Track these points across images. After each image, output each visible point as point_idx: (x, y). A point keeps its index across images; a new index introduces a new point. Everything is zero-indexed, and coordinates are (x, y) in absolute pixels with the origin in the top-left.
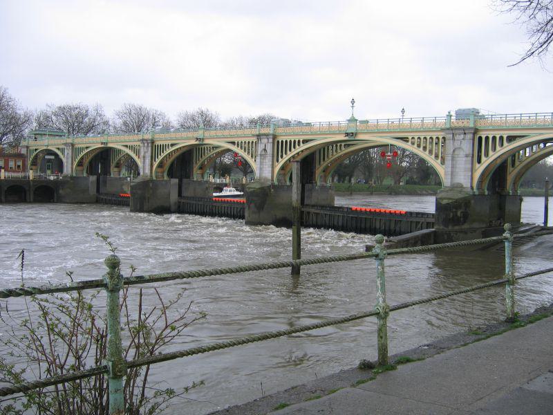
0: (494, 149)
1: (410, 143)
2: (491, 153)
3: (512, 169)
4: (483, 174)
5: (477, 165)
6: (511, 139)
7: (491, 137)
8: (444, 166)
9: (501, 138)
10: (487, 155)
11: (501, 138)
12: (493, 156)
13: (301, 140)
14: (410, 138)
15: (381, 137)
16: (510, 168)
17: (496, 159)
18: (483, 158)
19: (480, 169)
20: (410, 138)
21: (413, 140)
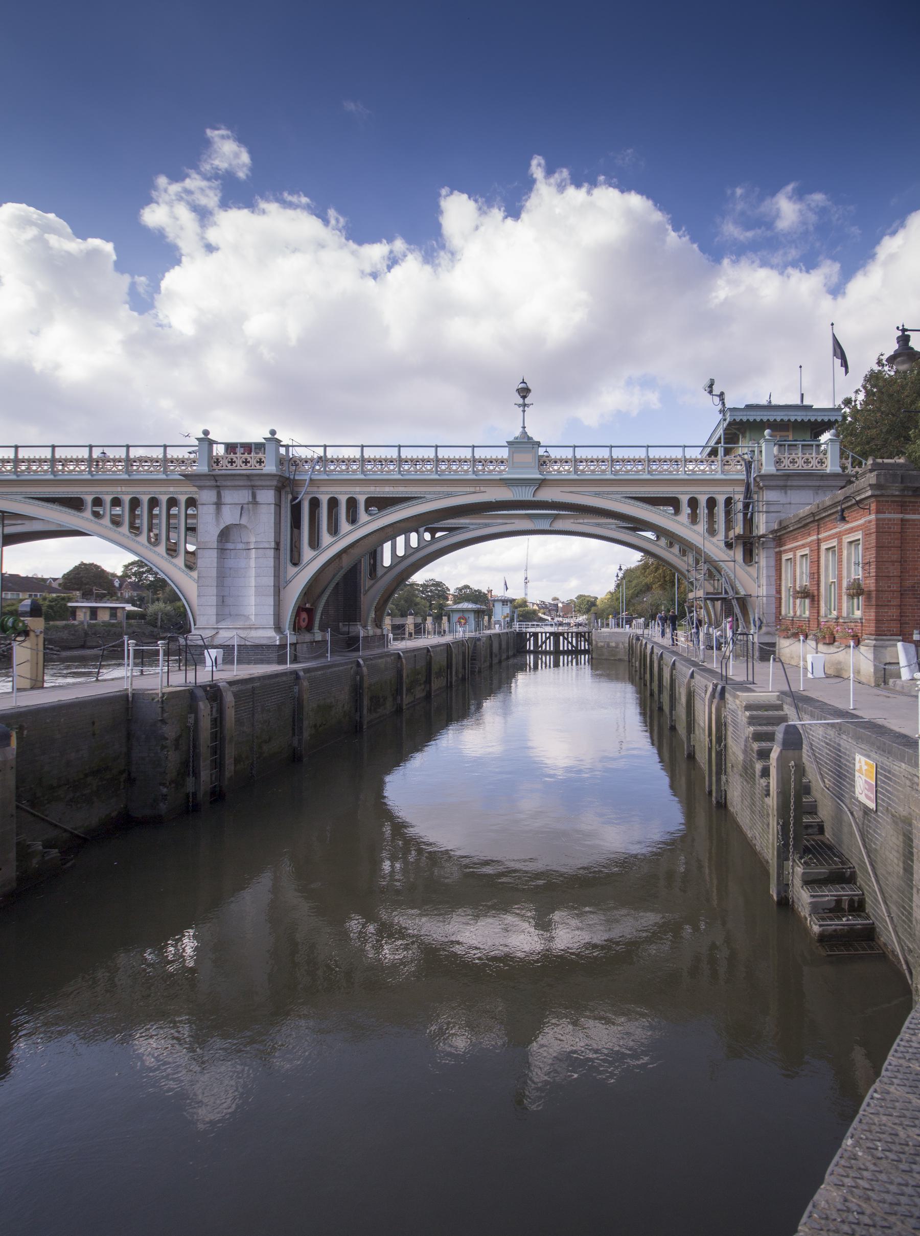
0: (334, 529)
1: (88, 514)
2: (326, 538)
3: (368, 583)
4: (310, 592)
5: (292, 570)
6: (380, 504)
7: (343, 499)
8: (195, 574)
9: (352, 503)
10: (315, 543)
11: (352, 503)
12: (331, 546)
13: (362, 499)
14: (89, 499)
15: (597, 494)
16: (365, 581)
17: (339, 555)
18: (307, 553)
19: (300, 579)
20: (89, 499)
21: (117, 510)
